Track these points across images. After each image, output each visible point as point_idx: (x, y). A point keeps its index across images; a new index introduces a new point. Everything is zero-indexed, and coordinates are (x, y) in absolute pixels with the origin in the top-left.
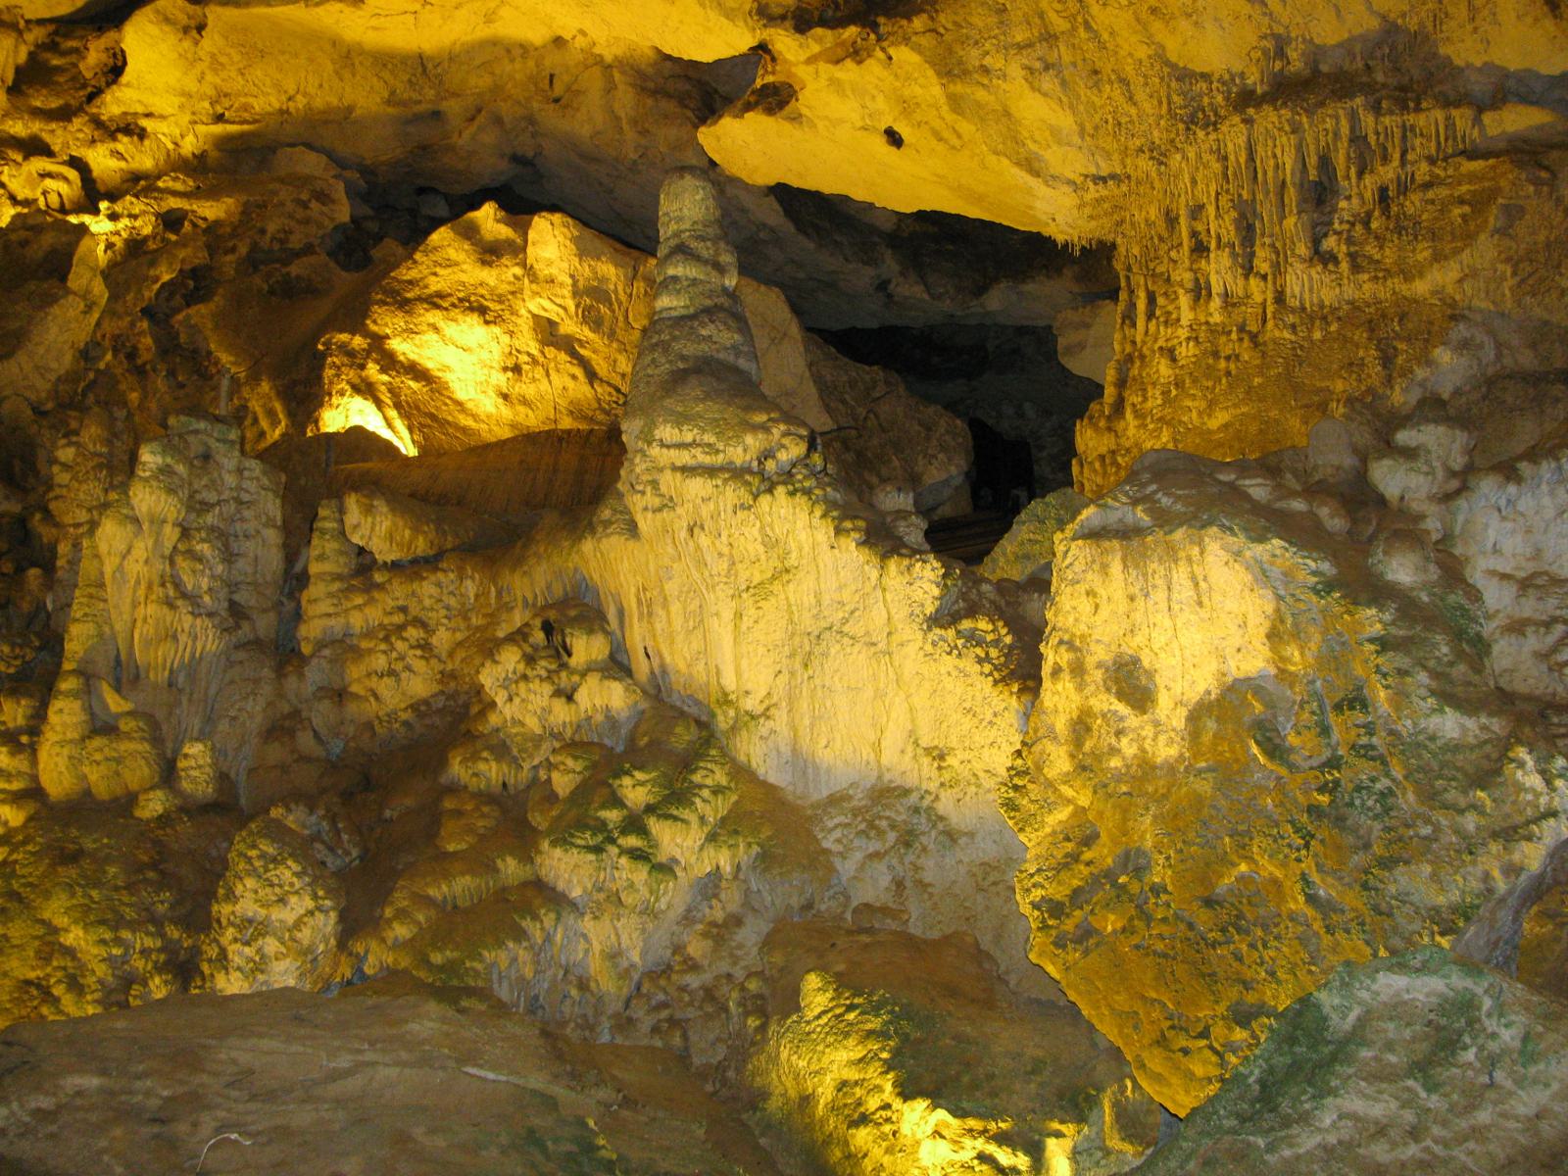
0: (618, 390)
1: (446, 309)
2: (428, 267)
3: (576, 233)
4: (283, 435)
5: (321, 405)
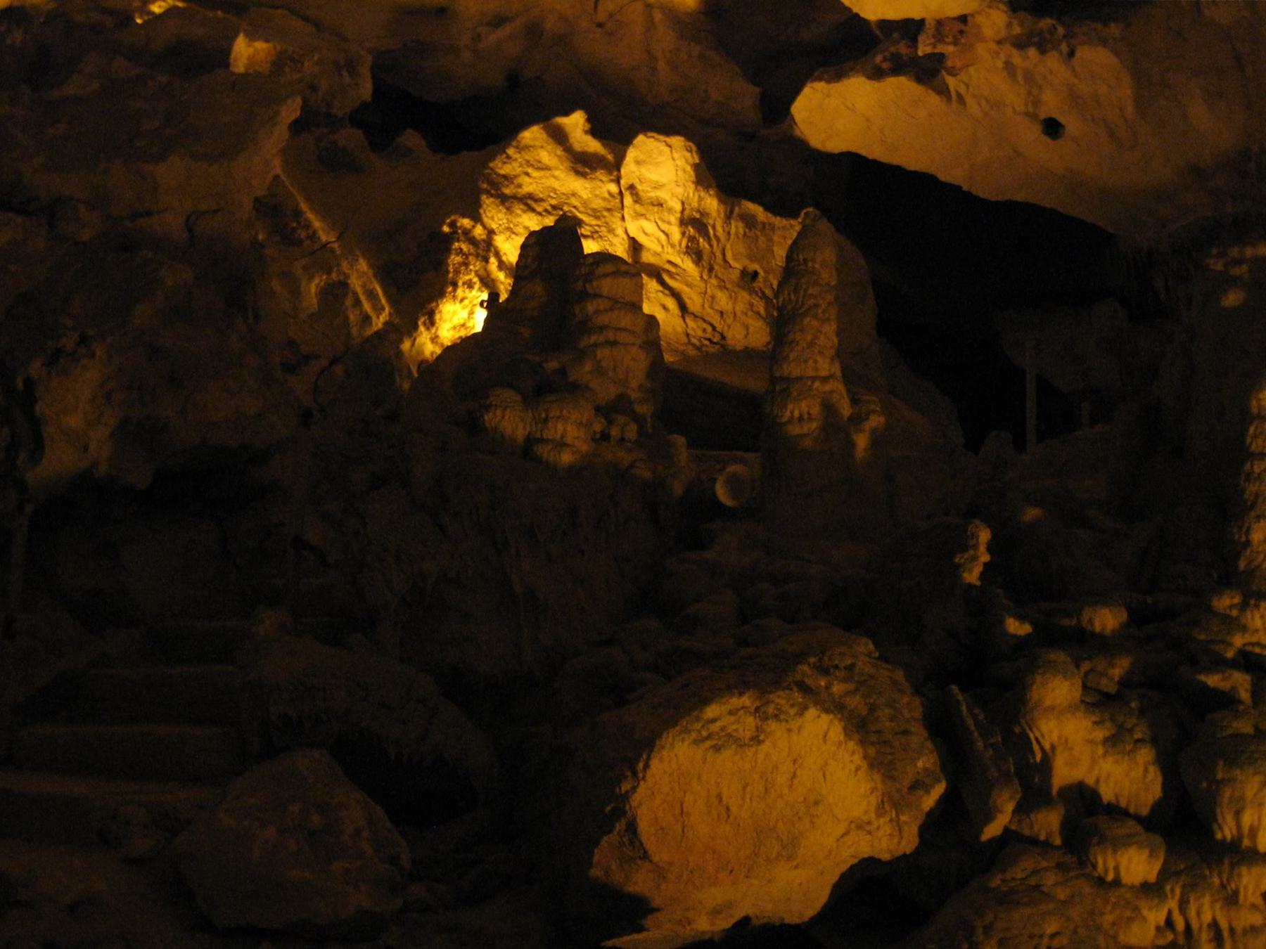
0: (714, 328)
1: (540, 214)
2: (521, 166)
3: (697, 161)
4: (386, 323)
5: (441, 295)
